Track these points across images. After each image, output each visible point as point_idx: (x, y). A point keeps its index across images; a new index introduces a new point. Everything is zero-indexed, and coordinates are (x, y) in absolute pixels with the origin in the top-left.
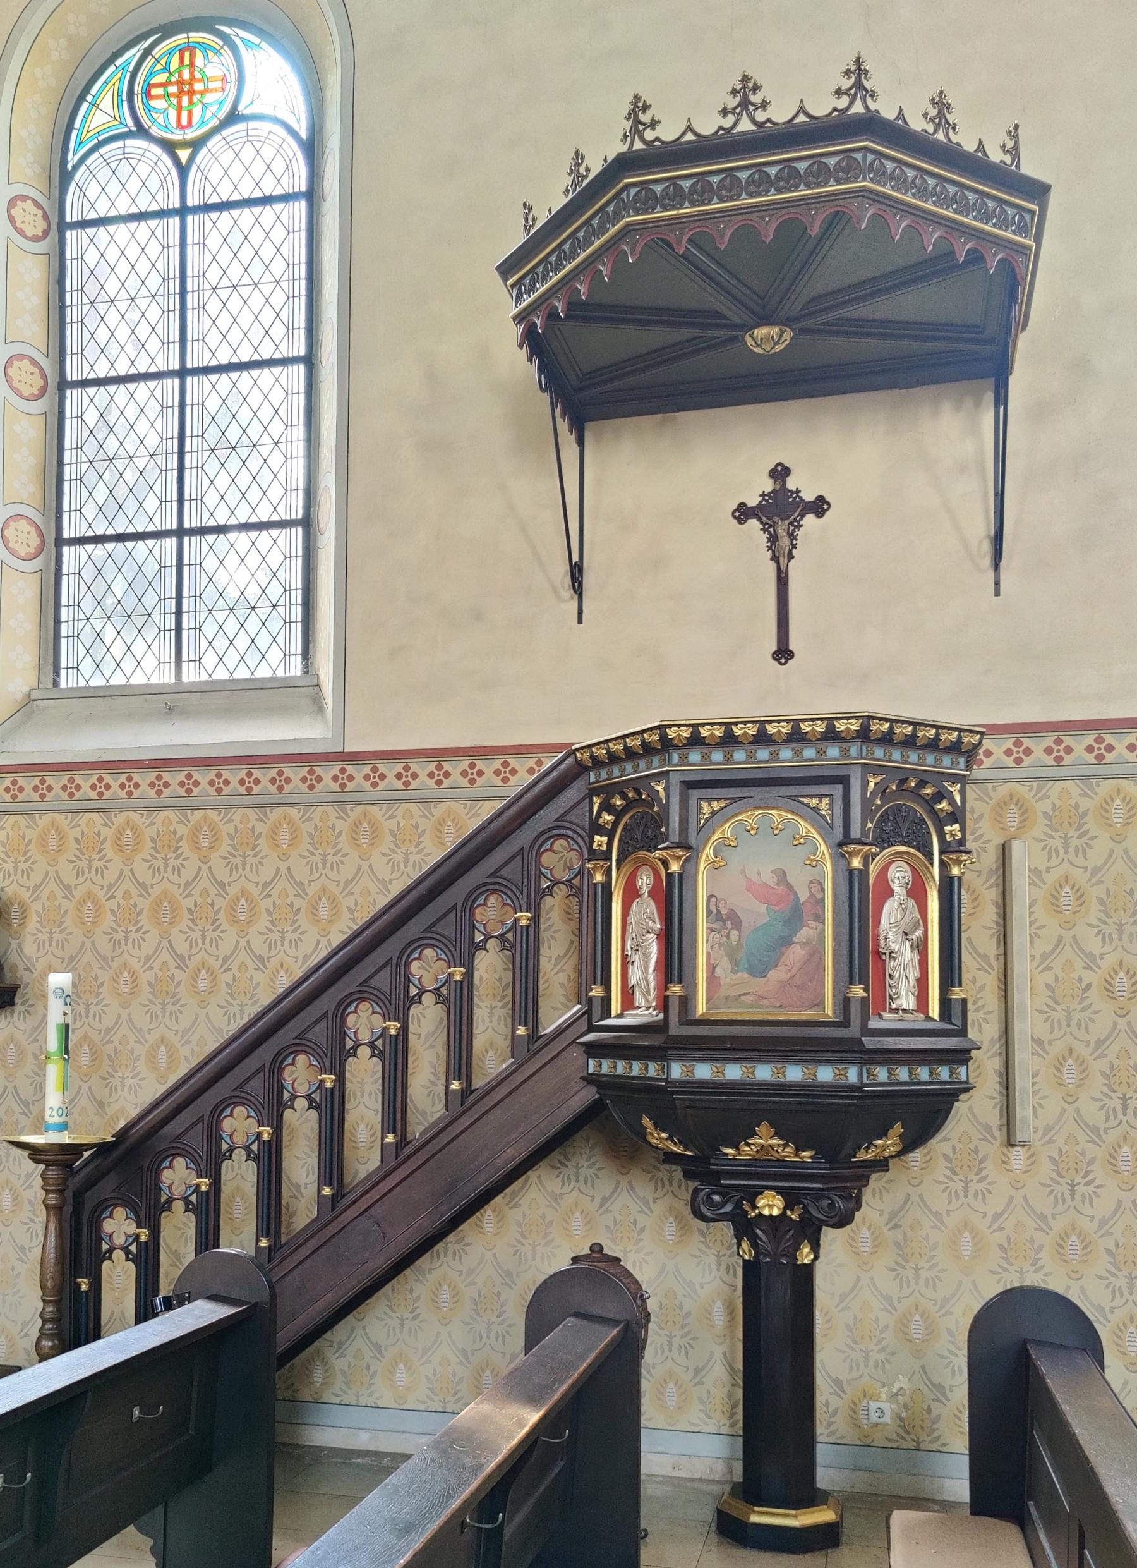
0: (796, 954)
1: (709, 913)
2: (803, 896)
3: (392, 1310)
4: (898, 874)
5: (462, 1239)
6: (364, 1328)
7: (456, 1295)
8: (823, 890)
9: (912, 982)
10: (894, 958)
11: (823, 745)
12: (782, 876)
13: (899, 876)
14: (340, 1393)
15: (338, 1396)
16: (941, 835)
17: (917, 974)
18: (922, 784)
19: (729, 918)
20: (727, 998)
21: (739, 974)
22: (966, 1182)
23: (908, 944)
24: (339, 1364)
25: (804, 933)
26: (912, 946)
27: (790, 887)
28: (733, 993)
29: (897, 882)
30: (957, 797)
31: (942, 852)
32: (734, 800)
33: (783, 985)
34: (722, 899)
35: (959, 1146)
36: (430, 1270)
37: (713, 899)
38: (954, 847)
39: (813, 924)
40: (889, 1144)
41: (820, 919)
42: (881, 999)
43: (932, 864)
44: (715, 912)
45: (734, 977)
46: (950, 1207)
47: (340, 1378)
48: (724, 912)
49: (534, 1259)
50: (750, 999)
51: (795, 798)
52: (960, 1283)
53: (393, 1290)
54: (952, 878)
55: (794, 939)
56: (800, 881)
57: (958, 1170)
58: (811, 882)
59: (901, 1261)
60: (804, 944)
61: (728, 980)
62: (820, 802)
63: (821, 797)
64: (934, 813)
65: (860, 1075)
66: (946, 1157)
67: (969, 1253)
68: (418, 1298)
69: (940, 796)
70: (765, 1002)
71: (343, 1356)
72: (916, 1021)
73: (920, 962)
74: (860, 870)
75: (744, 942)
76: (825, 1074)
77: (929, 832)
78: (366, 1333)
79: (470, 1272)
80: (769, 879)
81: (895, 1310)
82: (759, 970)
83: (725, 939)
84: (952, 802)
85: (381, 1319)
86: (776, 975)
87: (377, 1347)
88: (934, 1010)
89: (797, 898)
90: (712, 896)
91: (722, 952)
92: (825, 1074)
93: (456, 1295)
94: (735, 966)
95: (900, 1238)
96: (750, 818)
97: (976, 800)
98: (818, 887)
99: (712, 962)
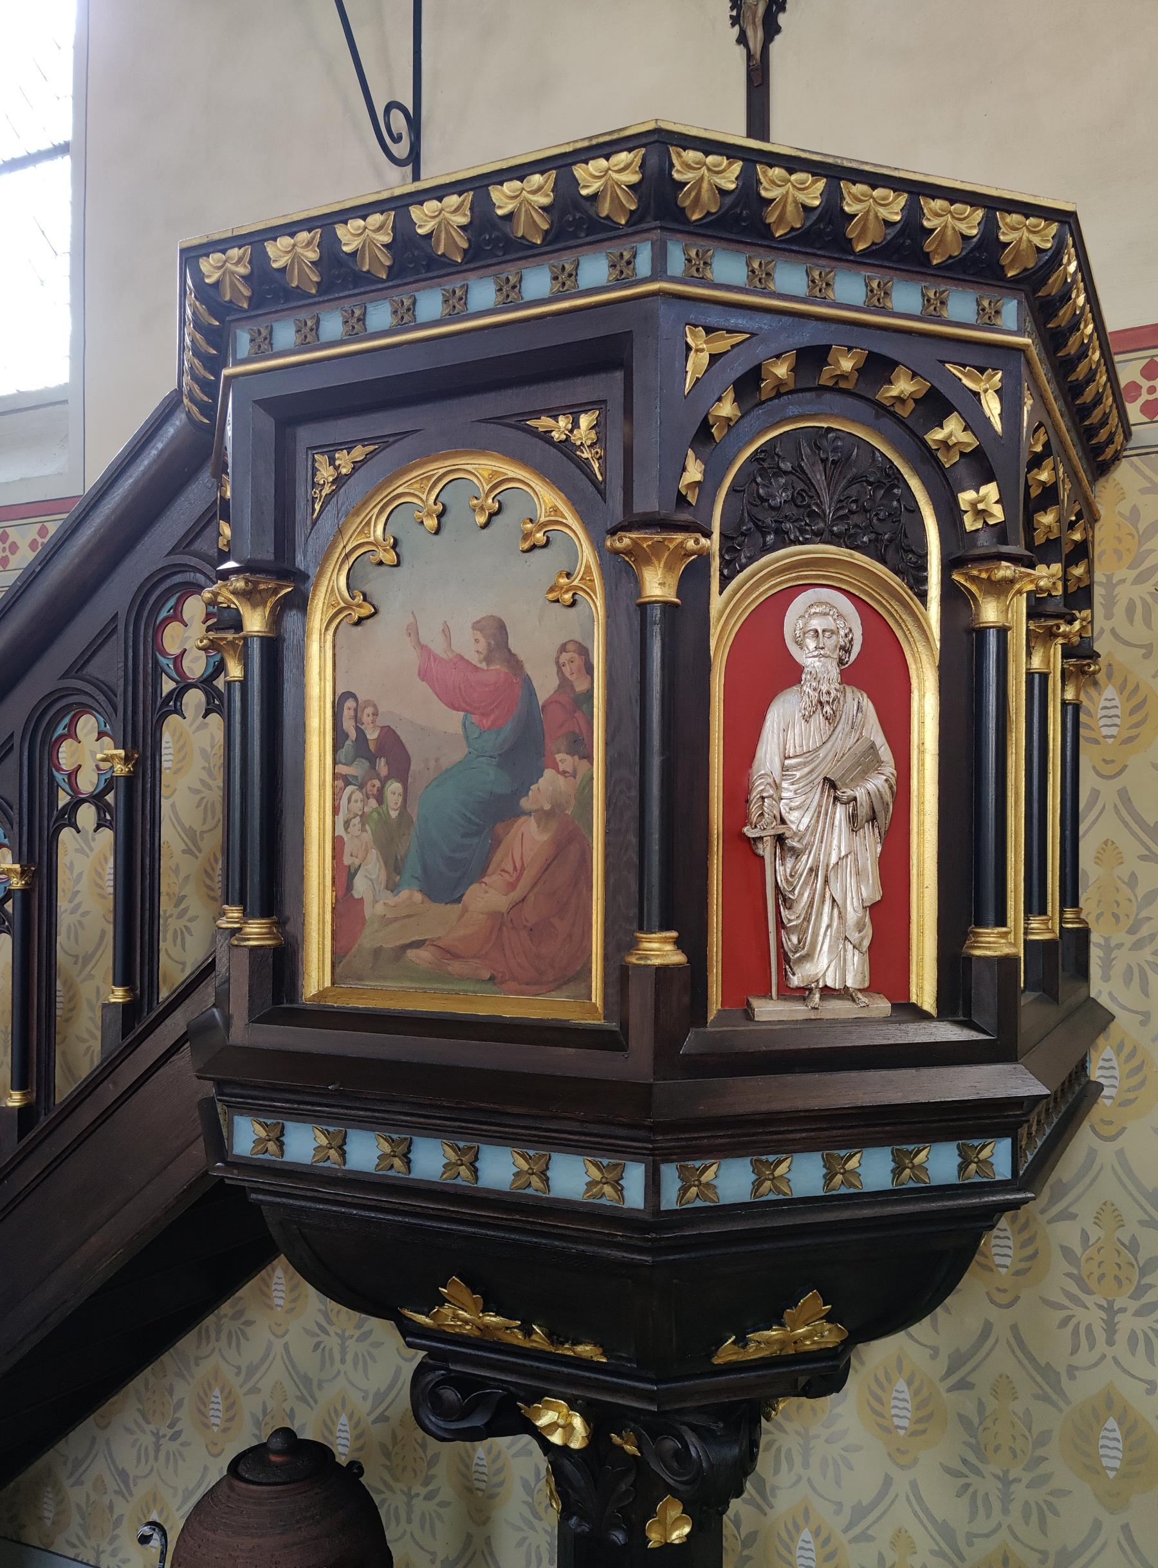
0: (529, 839)
1: (339, 737)
2: (545, 686)
3: (145, 1418)
4: (816, 623)
5: (240, 1313)
6: (108, 1443)
7: (231, 1406)
8: (589, 669)
9: (853, 912)
10: (796, 853)
11: (566, 260)
12: (497, 633)
13: (820, 627)
14: (76, 1542)
15: (74, 1546)
16: (949, 515)
17: (871, 891)
18: (878, 368)
19: (382, 750)
20: (377, 952)
21: (404, 894)
22: (1110, 1311)
23: (840, 812)
24: (76, 1495)
25: (548, 786)
26: (853, 819)
27: (515, 664)
28: (390, 940)
29: (811, 644)
30: (992, 407)
31: (950, 564)
32: (384, 442)
33: (499, 922)
34: (368, 703)
35: (1095, 1233)
36: (198, 1360)
37: (350, 703)
38: (985, 543)
39: (565, 761)
40: (808, 1328)
41: (581, 747)
42: (763, 959)
43: (923, 596)
44: (353, 734)
45: (392, 900)
46: (1077, 1360)
47: (76, 1519)
48: (372, 735)
49: (343, 1361)
50: (422, 957)
51: (518, 422)
52: (1097, 1526)
53: (146, 1386)
54: (981, 633)
55: (525, 803)
56: (537, 643)
57: (1093, 1284)
58: (563, 648)
59: (972, 1459)
60: (544, 817)
61: (380, 909)
62: (576, 425)
63: (575, 411)
64: (927, 460)
65: (653, 1185)
66: (1067, 1252)
67: (1117, 1464)
68: (179, 1405)
69: (936, 405)
70: (456, 967)
71: (79, 1482)
72: (870, 1019)
73: (883, 862)
74: (666, 605)
75: (414, 811)
76: (571, 1177)
77: (915, 510)
78: (110, 1450)
79: (252, 1370)
80: (469, 646)
81: (962, 1558)
82: (445, 882)
83: (373, 803)
84: (976, 421)
85: (131, 1432)
86: (486, 897)
87: (123, 1475)
88: (924, 989)
89: (532, 693)
90: (349, 695)
91: (368, 836)
92: (571, 1177)
93: (231, 1406)
94: (395, 867)
95: (971, 1410)
96: (417, 488)
97: (1143, 491)
98: (579, 660)
99: (347, 861)
